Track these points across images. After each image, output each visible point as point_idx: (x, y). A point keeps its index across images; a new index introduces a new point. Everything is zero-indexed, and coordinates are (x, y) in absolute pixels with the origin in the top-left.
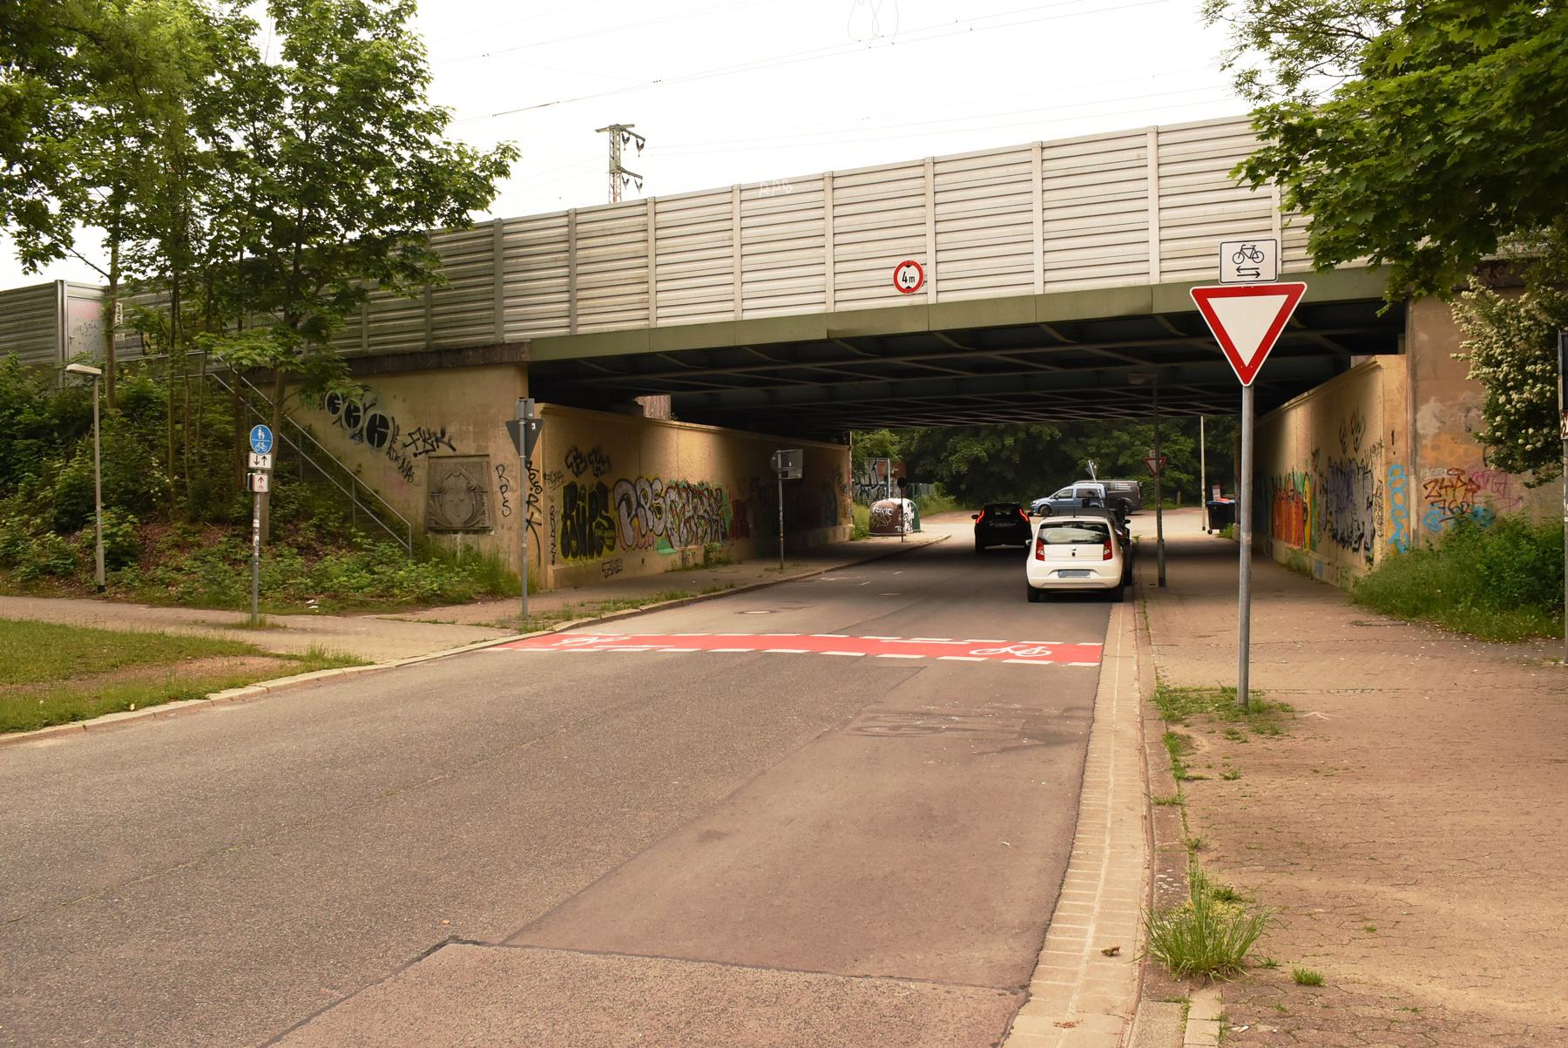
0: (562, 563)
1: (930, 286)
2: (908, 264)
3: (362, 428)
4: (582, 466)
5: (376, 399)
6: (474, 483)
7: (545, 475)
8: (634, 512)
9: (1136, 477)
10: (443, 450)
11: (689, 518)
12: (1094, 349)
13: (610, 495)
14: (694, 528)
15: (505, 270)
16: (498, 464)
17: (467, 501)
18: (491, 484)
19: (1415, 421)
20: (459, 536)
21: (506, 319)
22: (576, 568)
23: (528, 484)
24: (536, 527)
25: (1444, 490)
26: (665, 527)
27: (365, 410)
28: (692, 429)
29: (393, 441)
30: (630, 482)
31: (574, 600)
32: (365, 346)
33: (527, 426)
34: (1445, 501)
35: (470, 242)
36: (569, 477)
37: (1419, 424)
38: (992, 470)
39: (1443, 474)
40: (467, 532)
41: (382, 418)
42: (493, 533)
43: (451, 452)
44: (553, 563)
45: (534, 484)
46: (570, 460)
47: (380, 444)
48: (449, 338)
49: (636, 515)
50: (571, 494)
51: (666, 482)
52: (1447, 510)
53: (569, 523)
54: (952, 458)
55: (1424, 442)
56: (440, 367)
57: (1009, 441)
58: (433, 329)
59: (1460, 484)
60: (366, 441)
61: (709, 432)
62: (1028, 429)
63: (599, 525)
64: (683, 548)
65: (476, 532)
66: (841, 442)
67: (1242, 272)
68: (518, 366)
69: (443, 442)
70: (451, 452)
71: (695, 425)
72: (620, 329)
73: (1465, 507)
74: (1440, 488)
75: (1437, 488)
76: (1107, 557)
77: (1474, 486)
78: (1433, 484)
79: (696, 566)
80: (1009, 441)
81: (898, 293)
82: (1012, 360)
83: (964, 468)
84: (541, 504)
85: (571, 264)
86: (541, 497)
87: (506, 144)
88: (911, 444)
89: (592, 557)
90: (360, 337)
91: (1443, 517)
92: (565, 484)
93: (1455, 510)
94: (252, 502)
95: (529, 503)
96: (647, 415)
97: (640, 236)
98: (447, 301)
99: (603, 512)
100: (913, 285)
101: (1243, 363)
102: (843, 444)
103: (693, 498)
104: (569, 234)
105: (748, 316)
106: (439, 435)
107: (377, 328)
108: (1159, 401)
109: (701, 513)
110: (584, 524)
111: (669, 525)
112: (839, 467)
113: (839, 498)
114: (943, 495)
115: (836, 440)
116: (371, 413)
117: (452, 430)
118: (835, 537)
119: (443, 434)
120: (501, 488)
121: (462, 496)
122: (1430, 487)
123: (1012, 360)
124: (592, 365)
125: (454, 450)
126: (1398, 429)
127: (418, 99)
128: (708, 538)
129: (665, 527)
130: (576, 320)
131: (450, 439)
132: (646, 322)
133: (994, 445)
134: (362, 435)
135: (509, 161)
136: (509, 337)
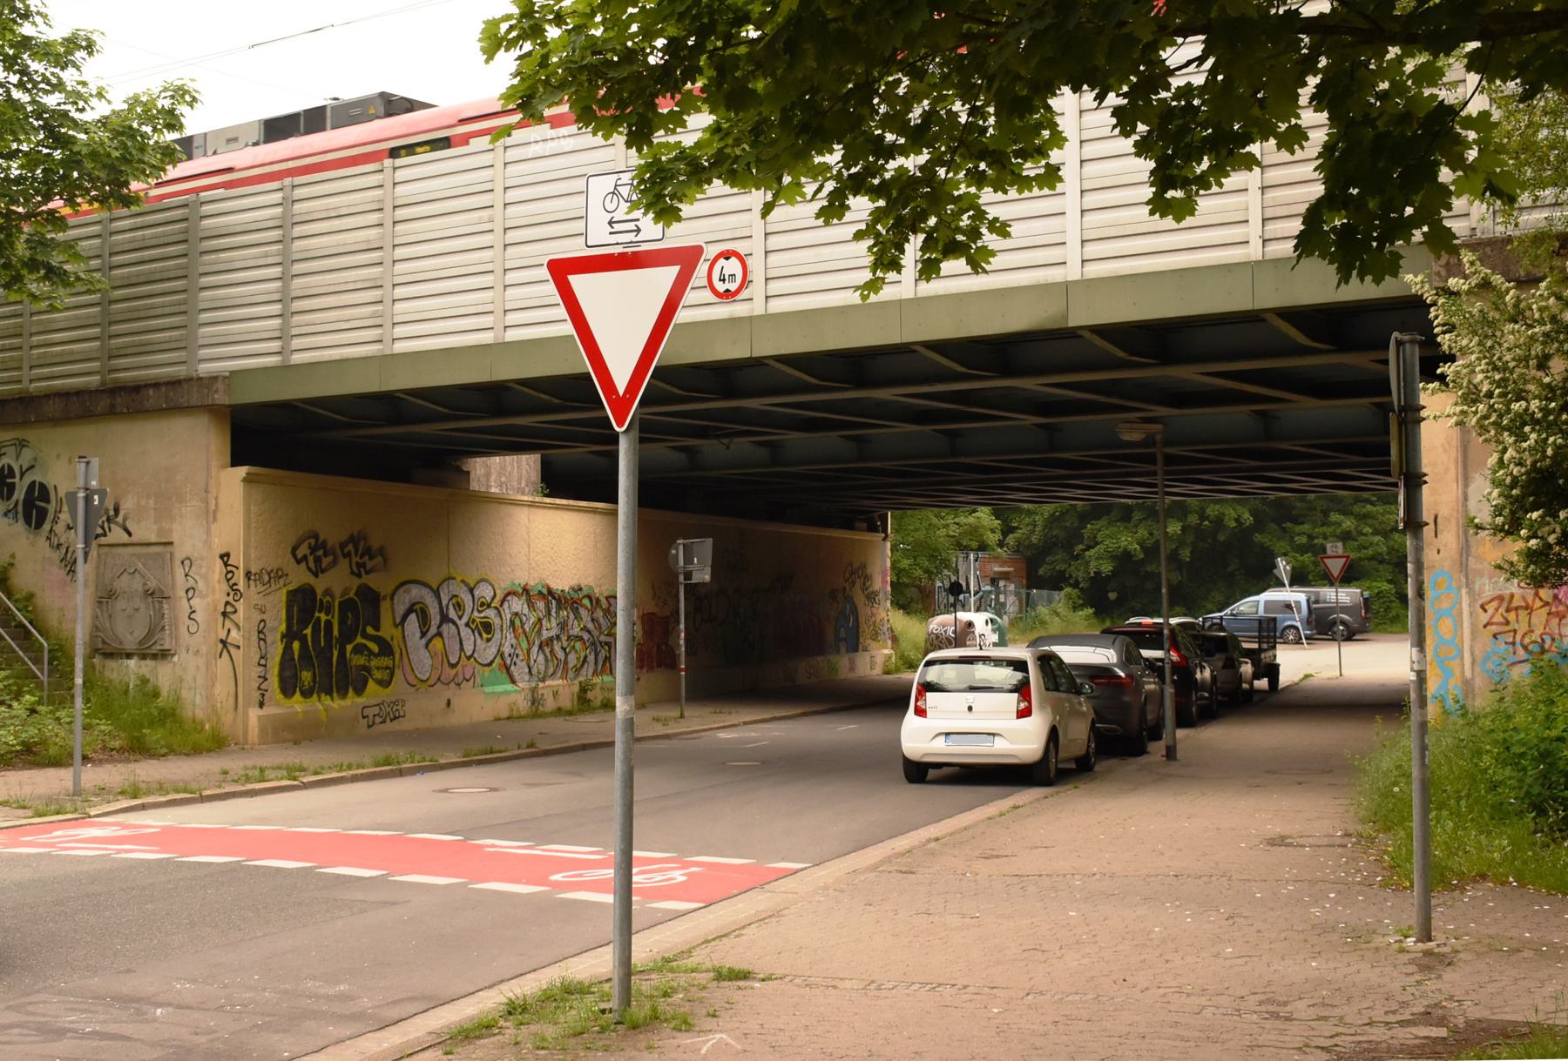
0: (278, 704)
1: (756, 289)
2: (727, 255)
3: (17, 501)
4: (326, 561)
5: (35, 459)
6: (152, 584)
7: (248, 574)
8: (433, 630)
9: (1357, 583)
10: (117, 535)
11: (551, 639)
13: (385, 606)
14: (561, 655)
15: (202, 269)
16: (184, 556)
17: (143, 609)
18: (173, 586)
20: (132, 663)
21: (201, 342)
22: (305, 713)
23: (226, 587)
24: (233, 650)
25: (1513, 613)
26: (500, 654)
27: (22, 474)
29: (55, 521)
30: (430, 587)
31: (292, 757)
32: (25, 384)
33: (88, 499)
34: (1515, 631)
35: (160, 229)
36: (299, 576)
38: (1149, 569)
40: (143, 657)
41: (42, 486)
42: (176, 659)
43: (125, 538)
44: (261, 705)
45: (231, 587)
46: (303, 550)
47: (39, 525)
48: (131, 370)
49: (439, 634)
50: (302, 604)
51: (503, 586)
52: (1518, 646)
53: (296, 645)
54: (1092, 552)
56: (112, 413)
57: (1174, 528)
58: (110, 358)
59: (1538, 603)
60: (21, 520)
61: (594, 511)
62: (1203, 510)
63: (359, 649)
64: (533, 685)
65: (154, 657)
66: (872, 528)
67: (617, 227)
68: (213, 410)
69: (117, 523)
70: (125, 538)
71: (564, 502)
72: (345, 356)
73: (1548, 641)
74: (1508, 610)
75: (1502, 610)
76: (1024, 713)
77: (1561, 608)
78: (1495, 604)
79: (559, 712)
80: (1174, 528)
81: (714, 299)
82: (903, 399)
83: (1107, 568)
84: (240, 616)
85: (286, 261)
86: (240, 606)
87: (179, 83)
88: (1032, 532)
89: (343, 694)
90: (19, 368)
92: (291, 588)
93: (1531, 647)
95: (224, 614)
96: (474, 486)
97: (373, 218)
98: (128, 316)
99: (370, 630)
100: (733, 287)
101: (616, 392)
102: (877, 531)
103: (559, 608)
104: (283, 216)
105: (513, 335)
106: (112, 513)
107: (40, 356)
108: (1166, 473)
109: (576, 631)
110: (329, 646)
111: (507, 650)
112: (864, 566)
113: (864, 611)
114: (1075, 608)
115: (864, 525)
116: (28, 479)
117: (127, 505)
118: (852, 669)
119: (117, 511)
120: (187, 592)
121: (138, 603)
122: (1491, 608)
123: (903, 399)
124: (307, 407)
125: (130, 534)
127: (38, 19)
128: (589, 669)
129: (500, 654)
130: (289, 344)
131: (125, 520)
133: (1151, 534)
134: (17, 513)
135: (182, 109)
136: (205, 369)
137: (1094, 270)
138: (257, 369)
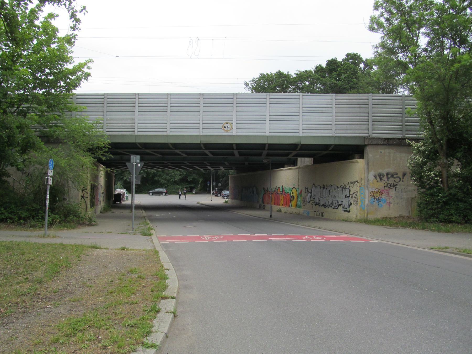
12: (147, 151)
19: (368, 176)
24: (85, 198)
28: (286, 170)
37: (369, 177)
39: (374, 190)
55: (370, 182)
91: (374, 201)
94: (47, 188)
126: (362, 178)
132: (265, 133)
137: (171, 134)
138: (160, 135)
